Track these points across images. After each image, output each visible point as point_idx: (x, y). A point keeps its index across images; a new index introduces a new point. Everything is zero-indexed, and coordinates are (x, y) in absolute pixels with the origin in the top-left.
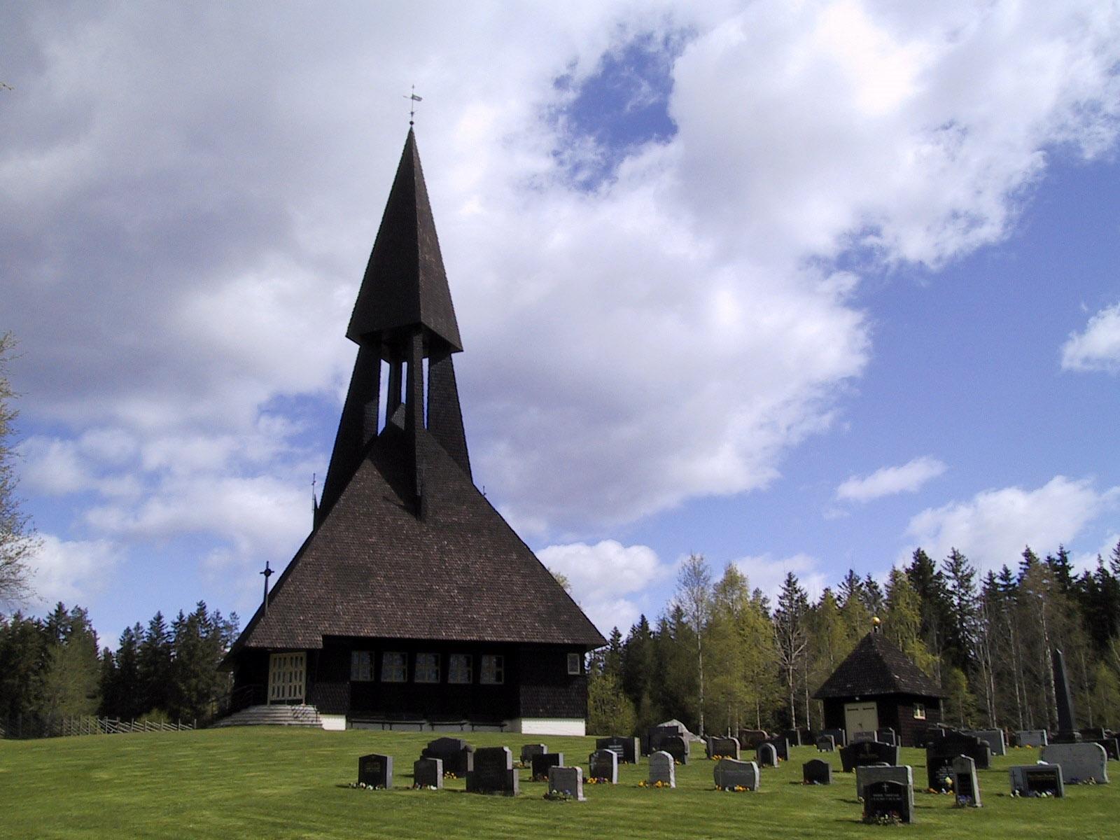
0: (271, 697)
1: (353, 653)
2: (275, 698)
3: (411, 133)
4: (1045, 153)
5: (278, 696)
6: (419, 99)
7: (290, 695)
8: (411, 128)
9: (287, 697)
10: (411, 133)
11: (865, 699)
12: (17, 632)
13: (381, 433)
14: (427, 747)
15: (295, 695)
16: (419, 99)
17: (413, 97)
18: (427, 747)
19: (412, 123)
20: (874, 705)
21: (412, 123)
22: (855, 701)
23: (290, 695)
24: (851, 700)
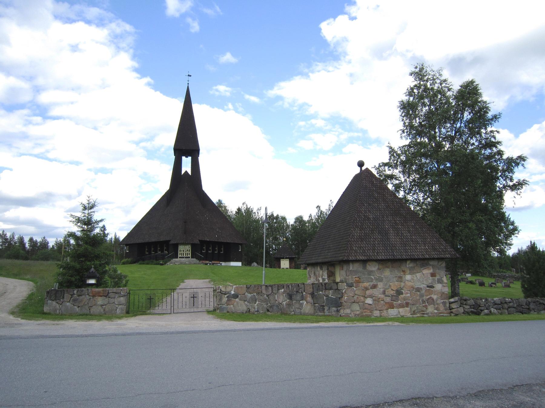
0: (179, 256)
1: (511, 255)
2: (181, 256)
3: (188, 87)
4: (307, 113)
5: (182, 255)
6: (190, 76)
7: (186, 255)
8: (188, 85)
9: (185, 256)
10: (188, 87)
11: (286, 258)
12: (468, 151)
13: (191, 174)
14: (171, 260)
15: (187, 255)
16: (190, 76)
17: (189, 75)
18: (171, 260)
19: (188, 84)
20: (288, 260)
21: (188, 84)
22: (284, 259)
23: (186, 255)
24: (283, 258)
